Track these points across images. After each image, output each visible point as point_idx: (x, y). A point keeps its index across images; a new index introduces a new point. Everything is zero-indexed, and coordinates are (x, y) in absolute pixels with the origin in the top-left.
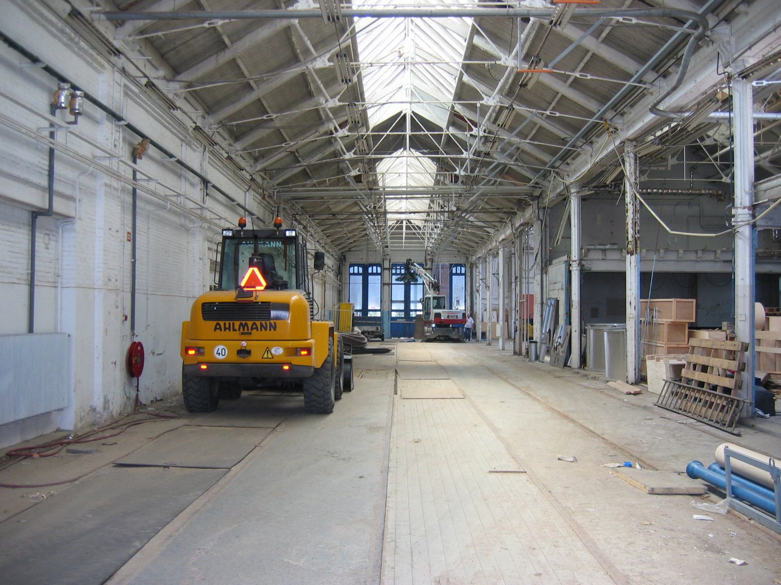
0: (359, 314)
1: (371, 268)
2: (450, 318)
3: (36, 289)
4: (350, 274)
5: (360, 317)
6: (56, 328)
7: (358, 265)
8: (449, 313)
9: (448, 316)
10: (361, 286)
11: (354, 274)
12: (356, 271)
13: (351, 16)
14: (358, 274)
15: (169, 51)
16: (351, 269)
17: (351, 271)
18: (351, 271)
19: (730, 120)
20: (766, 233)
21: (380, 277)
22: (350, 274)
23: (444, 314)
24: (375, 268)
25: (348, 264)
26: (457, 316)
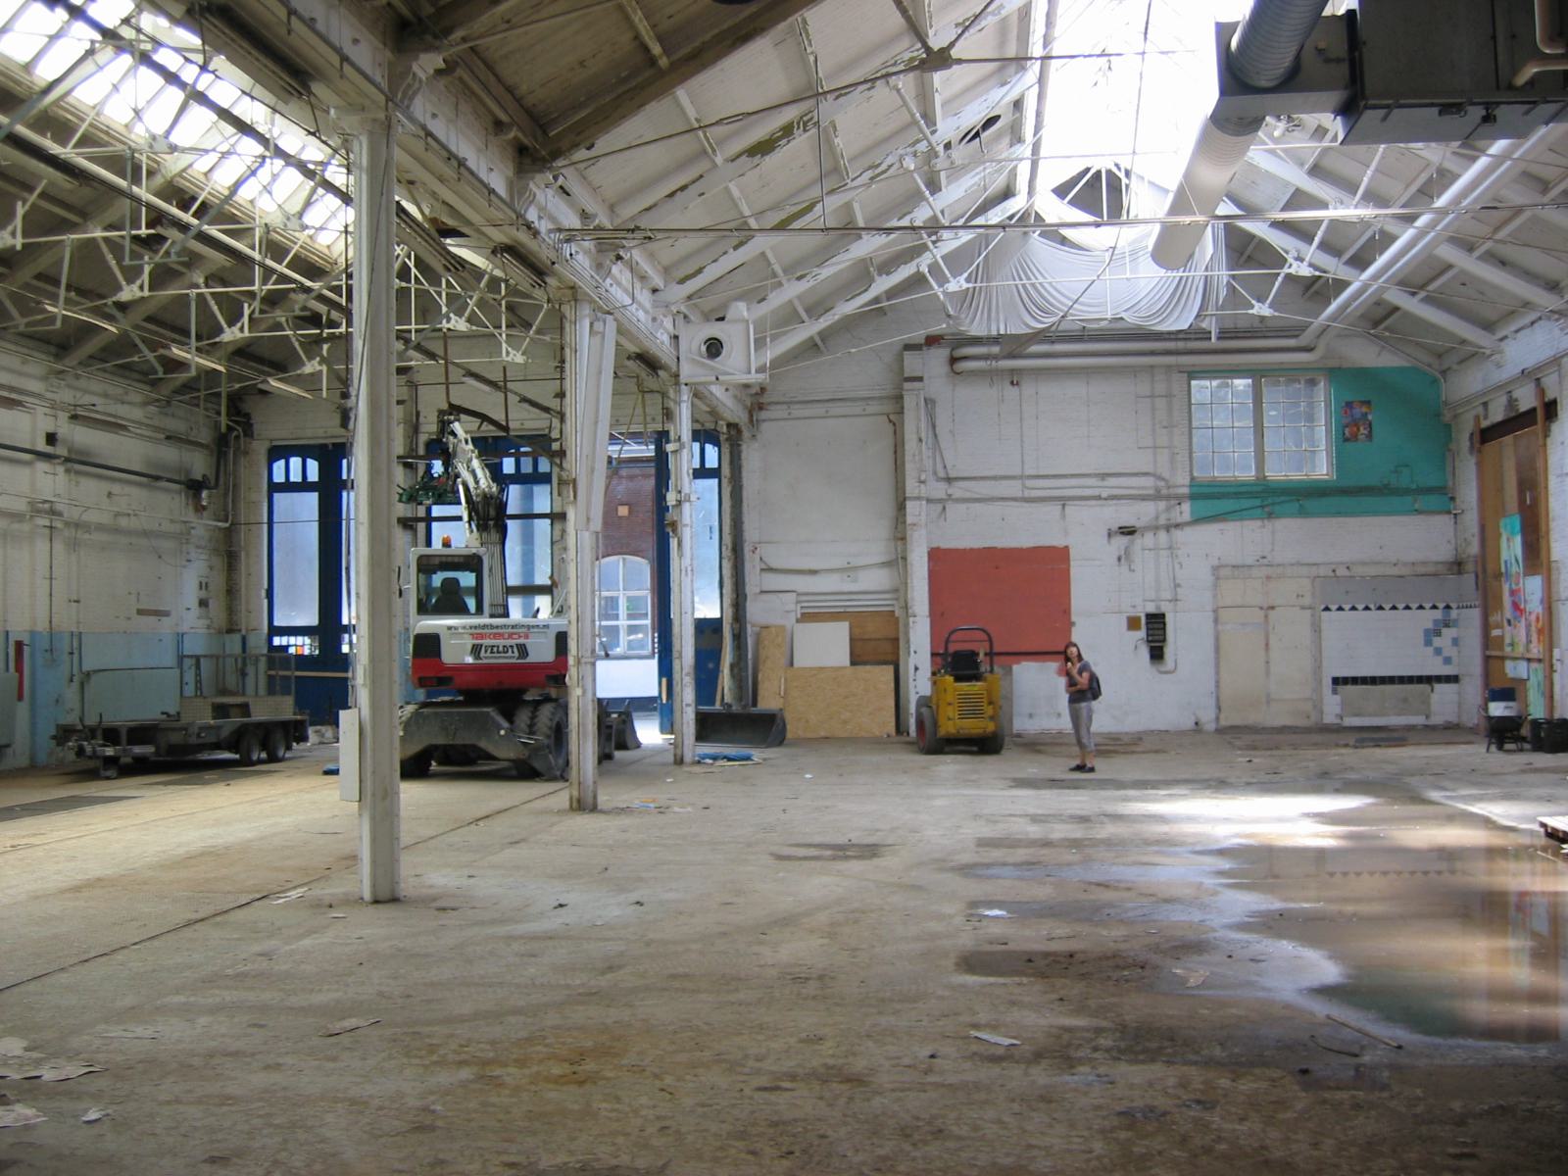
0: (302, 645)
1: (281, 463)
2: (487, 659)
3: (276, 526)
4: (274, 488)
5: (311, 656)
6: (1155, 454)
7: (304, 452)
8: (477, 632)
9: (476, 650)
10: (315, 528)
11: (288, 487)
12: (296, 477)
13: (1503, 658)
14: (304, 486)
15: (238, 185)
16: (279, 467)
17: (279, 477)
18: (279, 477)
19: (780, 284)
20: (189, 12)
21: (715, 482)
22: (274, 488)
23: (457, 636)
24: (295, 462)
25: (260, 448)
26: (523, 650)
